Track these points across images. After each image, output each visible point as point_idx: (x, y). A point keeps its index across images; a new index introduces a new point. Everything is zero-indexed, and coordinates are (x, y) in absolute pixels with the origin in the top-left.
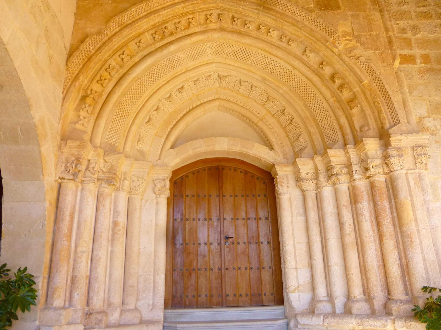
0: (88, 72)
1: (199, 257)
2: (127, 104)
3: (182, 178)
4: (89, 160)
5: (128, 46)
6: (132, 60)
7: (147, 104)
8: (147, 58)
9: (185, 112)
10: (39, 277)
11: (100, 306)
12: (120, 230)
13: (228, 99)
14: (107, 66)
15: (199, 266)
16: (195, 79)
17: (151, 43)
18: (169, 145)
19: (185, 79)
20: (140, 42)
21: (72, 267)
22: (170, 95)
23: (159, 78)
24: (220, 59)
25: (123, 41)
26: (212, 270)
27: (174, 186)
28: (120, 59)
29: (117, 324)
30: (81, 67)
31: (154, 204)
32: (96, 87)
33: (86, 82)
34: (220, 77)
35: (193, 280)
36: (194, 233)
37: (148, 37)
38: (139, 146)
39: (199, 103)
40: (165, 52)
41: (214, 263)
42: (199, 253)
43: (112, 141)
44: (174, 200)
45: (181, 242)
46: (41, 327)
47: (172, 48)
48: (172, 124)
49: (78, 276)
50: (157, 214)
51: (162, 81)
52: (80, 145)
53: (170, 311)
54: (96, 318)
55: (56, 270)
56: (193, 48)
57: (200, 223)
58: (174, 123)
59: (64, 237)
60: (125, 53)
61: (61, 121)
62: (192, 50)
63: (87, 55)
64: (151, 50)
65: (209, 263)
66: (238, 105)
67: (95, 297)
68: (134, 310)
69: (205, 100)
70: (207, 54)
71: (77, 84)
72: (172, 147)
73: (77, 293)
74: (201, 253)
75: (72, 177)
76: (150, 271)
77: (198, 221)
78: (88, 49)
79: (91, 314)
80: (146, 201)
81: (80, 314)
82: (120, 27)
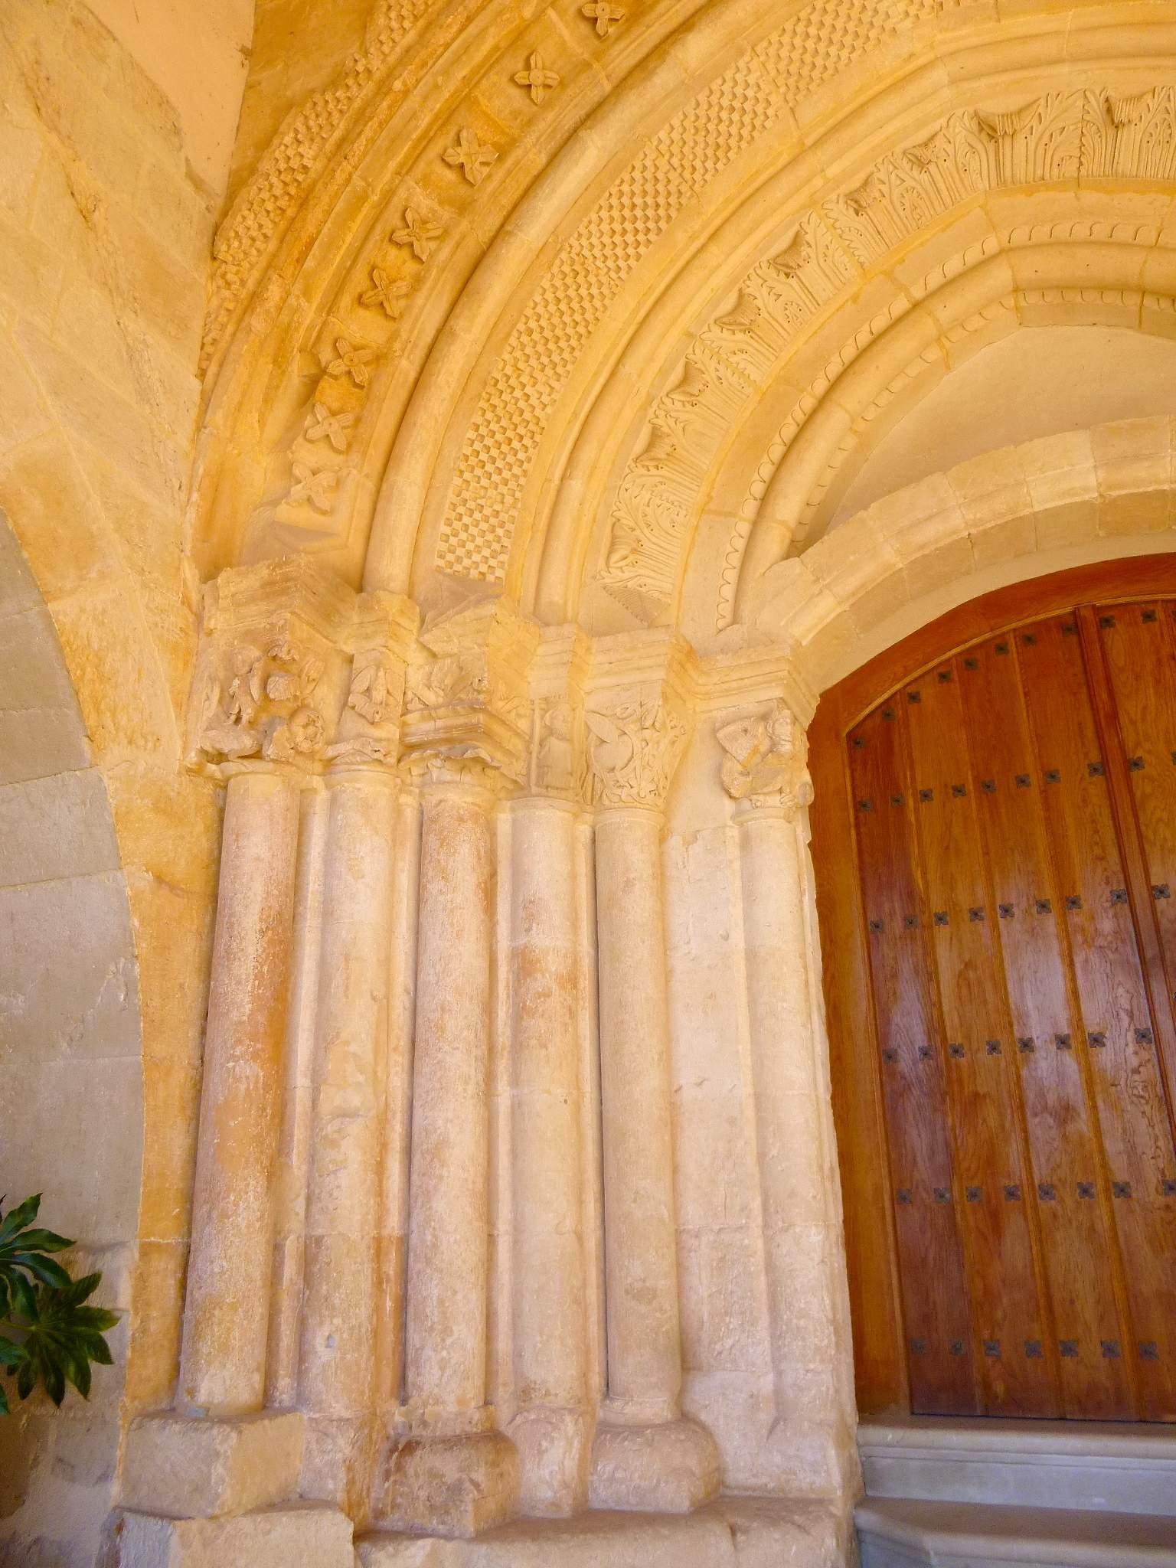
0: (310, 263)
1: (1033, 1122)
2: (524, 379)
3: (886, 711)
4: (351, 660)
5: (476, 102)
6: (509, 162)
7: (630, 367)
8: (582, 133)
9: (834, 368)
10: (122, 1244)
11: (461, 1402)
12: (547, 995)
13: (1062, 231)
14: (392, 218)
15: (1041, 1172)
16: (856, 183)
17: (586, 56)
18: (774, 541)
19: (802, 198)
20: (528, 67)
21: (304, 1192)
22: (741, 295)
23: (663, 224)
24: (965, 31)
25: (452, 87)
26: (1123, 1190)
27: (852, 761)
28: (450, 176)
29: (566, 1512)
30: (272, 246)
31: (733, 851)
32: (362, 328)
33: (311, 315)
34: (988, 129)
35: (1016, 1249)
36: (989, 986)
37: (566, 33)
38: (622, 574)
39: (901, 305)
40: (664, 78)
41: (1132, 1149)
42: (1031, 1096)
43: (466, 562)
44: (857, 826)
45: (921, 1041)
46: (127, 1515)
47: (696, 47)
48: (777, 440)
49: (327, 1241)
50: (750, 896)
51: (681, 236)
52: (272, 583)
53: (890, 1435)
54: (434, 1474)
55: (205, 1208)
56: (803, 15)
57: (1013, 930)
58: (789, 431)
59: (239, 1042)
60: (464, 134)
61: (195, 496)
62: (800, 28)
63: (293, 191)
64: (594, 96)
65: (1102, 1150)
66: (1123, 245)
67: (428, 1352)
68: (665, 1426)
69: (935, 280)
70: (888, 25)
71: (258, 323)
72: (797, 548)
73: (326, 1331)
74: (1041, 1094)
75: (247, 743)
76: (744, 1208)
77: (1002, 922)
78: (295, 163)
79: (411, 1447)
80: (692, 839)
81: (343, 1446)
82: (421, 23)
